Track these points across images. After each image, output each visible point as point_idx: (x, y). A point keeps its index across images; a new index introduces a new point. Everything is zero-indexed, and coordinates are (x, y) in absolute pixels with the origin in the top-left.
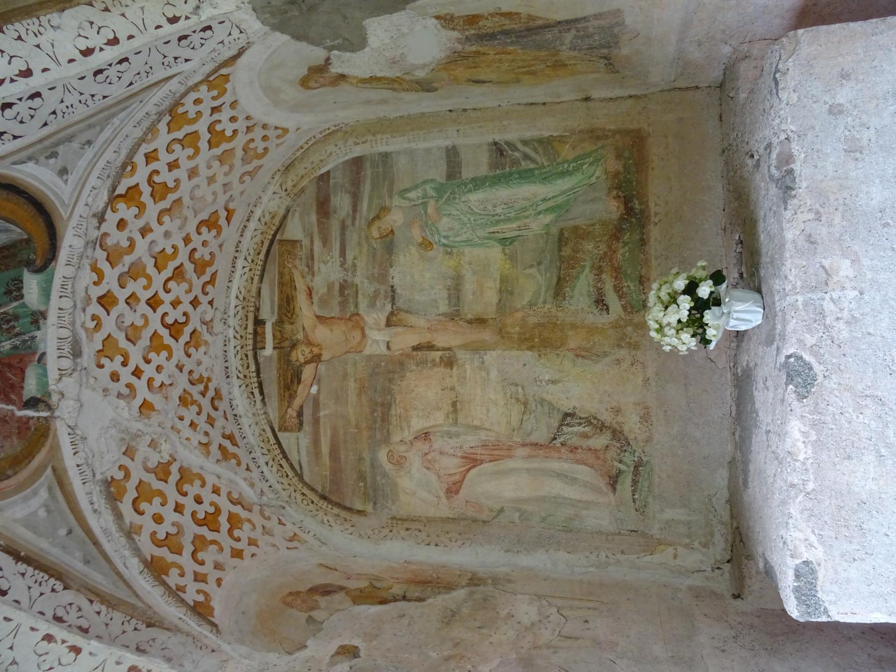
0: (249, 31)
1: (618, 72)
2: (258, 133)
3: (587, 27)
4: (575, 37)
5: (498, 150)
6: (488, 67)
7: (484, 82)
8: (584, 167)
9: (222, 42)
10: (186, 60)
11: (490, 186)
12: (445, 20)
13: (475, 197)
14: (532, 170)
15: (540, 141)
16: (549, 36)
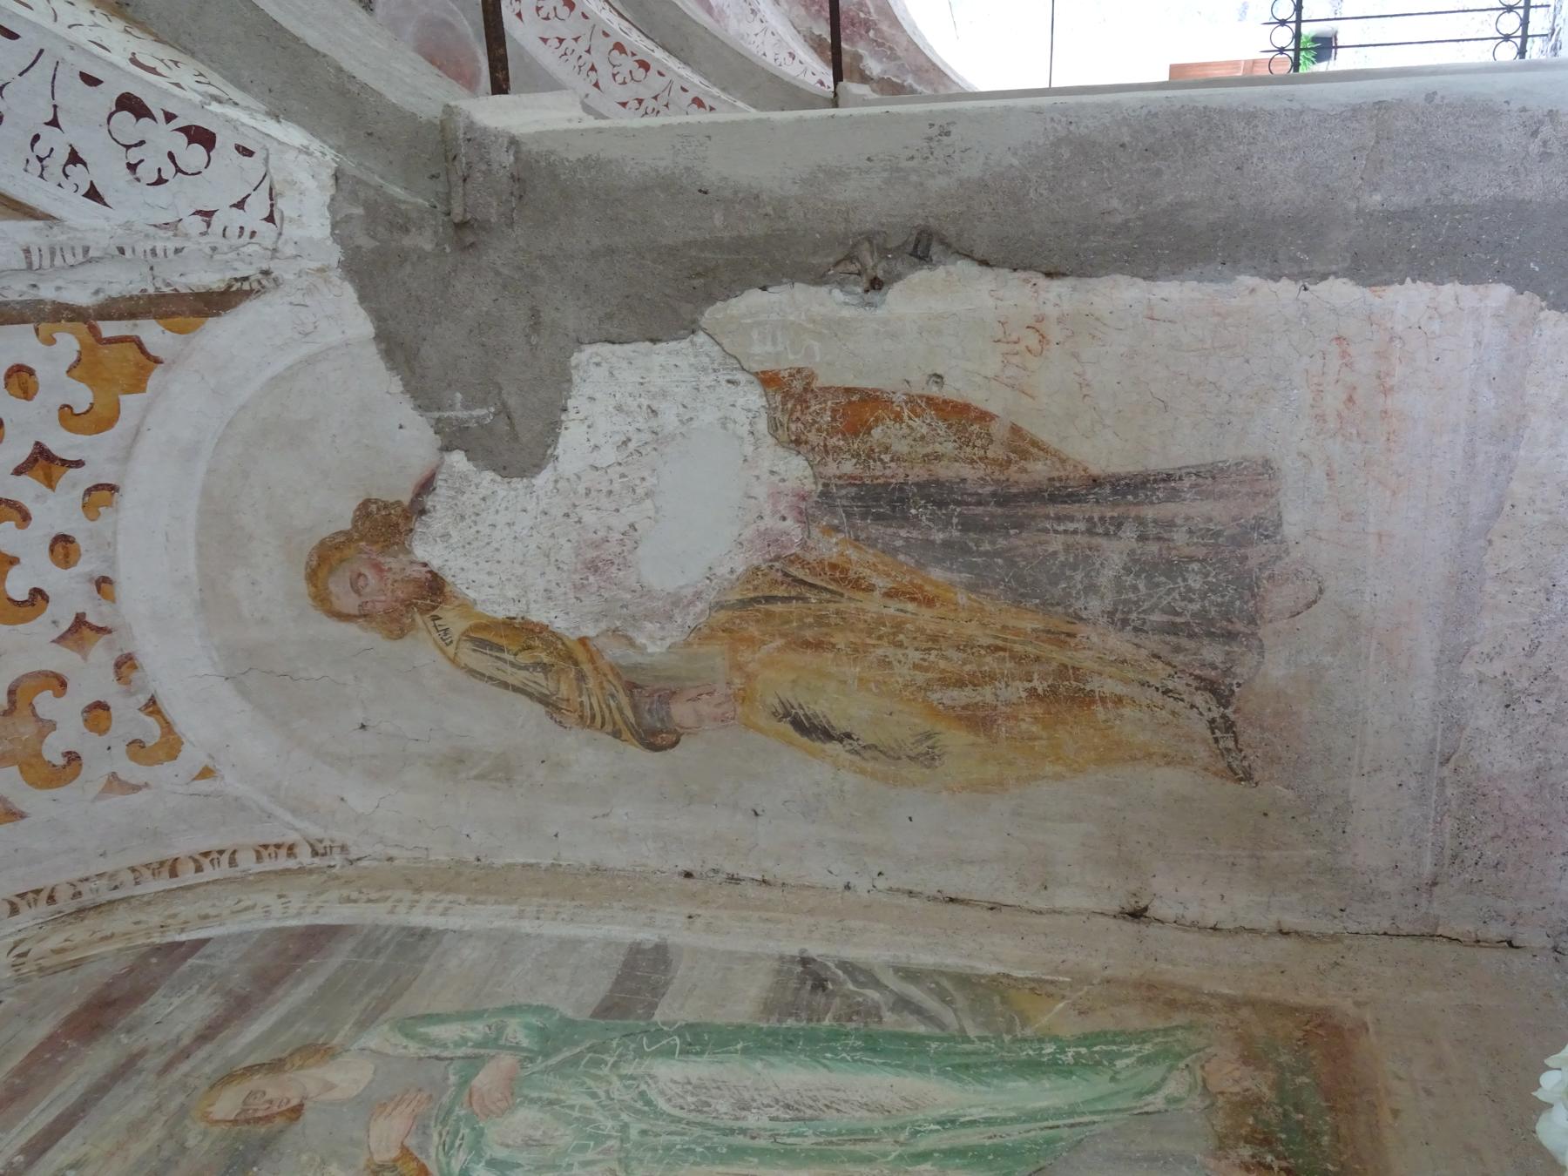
0: (290, 231)
1: (1248, 777)
2: (91, 675)
3: (1170, 524)
4: (1137, 565)
5: (812, 976)
6: (857, 651)
7: (827, 734)
8: (1119, 1064)
9: (207, 215)
10: (93, 194)
11: (745, 1051)
12: (787, 396)
13: (671, 1074)
14: (921, 1038)
15: (965, 981)
16: (1056, 544)
